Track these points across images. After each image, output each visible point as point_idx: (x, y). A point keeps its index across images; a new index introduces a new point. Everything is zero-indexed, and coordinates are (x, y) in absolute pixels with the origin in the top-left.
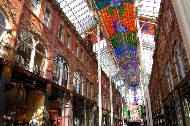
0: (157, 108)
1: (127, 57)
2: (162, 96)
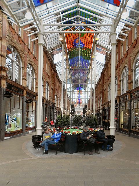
0: (98, 109)
1: (80, 63)
2: (103, 102)
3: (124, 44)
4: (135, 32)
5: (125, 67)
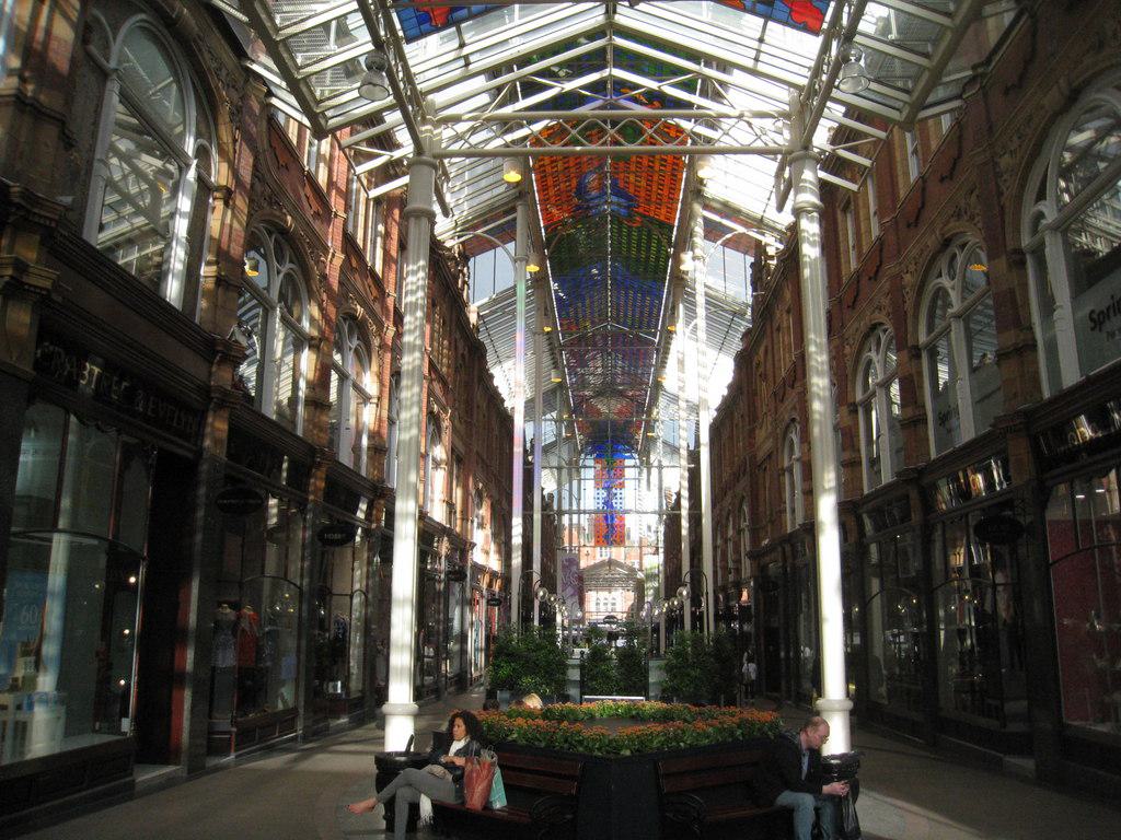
0: (725, 577)
3: (857, 206)
4: (910, 149)
5: (874, 327)
